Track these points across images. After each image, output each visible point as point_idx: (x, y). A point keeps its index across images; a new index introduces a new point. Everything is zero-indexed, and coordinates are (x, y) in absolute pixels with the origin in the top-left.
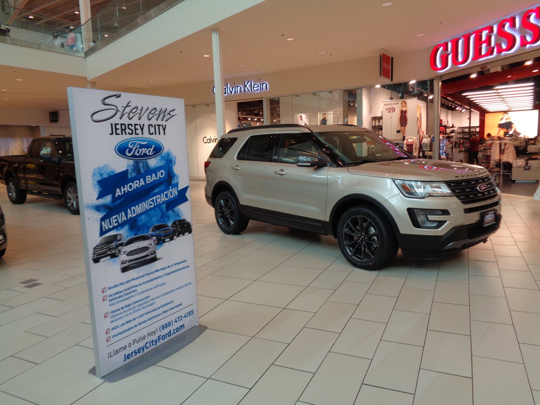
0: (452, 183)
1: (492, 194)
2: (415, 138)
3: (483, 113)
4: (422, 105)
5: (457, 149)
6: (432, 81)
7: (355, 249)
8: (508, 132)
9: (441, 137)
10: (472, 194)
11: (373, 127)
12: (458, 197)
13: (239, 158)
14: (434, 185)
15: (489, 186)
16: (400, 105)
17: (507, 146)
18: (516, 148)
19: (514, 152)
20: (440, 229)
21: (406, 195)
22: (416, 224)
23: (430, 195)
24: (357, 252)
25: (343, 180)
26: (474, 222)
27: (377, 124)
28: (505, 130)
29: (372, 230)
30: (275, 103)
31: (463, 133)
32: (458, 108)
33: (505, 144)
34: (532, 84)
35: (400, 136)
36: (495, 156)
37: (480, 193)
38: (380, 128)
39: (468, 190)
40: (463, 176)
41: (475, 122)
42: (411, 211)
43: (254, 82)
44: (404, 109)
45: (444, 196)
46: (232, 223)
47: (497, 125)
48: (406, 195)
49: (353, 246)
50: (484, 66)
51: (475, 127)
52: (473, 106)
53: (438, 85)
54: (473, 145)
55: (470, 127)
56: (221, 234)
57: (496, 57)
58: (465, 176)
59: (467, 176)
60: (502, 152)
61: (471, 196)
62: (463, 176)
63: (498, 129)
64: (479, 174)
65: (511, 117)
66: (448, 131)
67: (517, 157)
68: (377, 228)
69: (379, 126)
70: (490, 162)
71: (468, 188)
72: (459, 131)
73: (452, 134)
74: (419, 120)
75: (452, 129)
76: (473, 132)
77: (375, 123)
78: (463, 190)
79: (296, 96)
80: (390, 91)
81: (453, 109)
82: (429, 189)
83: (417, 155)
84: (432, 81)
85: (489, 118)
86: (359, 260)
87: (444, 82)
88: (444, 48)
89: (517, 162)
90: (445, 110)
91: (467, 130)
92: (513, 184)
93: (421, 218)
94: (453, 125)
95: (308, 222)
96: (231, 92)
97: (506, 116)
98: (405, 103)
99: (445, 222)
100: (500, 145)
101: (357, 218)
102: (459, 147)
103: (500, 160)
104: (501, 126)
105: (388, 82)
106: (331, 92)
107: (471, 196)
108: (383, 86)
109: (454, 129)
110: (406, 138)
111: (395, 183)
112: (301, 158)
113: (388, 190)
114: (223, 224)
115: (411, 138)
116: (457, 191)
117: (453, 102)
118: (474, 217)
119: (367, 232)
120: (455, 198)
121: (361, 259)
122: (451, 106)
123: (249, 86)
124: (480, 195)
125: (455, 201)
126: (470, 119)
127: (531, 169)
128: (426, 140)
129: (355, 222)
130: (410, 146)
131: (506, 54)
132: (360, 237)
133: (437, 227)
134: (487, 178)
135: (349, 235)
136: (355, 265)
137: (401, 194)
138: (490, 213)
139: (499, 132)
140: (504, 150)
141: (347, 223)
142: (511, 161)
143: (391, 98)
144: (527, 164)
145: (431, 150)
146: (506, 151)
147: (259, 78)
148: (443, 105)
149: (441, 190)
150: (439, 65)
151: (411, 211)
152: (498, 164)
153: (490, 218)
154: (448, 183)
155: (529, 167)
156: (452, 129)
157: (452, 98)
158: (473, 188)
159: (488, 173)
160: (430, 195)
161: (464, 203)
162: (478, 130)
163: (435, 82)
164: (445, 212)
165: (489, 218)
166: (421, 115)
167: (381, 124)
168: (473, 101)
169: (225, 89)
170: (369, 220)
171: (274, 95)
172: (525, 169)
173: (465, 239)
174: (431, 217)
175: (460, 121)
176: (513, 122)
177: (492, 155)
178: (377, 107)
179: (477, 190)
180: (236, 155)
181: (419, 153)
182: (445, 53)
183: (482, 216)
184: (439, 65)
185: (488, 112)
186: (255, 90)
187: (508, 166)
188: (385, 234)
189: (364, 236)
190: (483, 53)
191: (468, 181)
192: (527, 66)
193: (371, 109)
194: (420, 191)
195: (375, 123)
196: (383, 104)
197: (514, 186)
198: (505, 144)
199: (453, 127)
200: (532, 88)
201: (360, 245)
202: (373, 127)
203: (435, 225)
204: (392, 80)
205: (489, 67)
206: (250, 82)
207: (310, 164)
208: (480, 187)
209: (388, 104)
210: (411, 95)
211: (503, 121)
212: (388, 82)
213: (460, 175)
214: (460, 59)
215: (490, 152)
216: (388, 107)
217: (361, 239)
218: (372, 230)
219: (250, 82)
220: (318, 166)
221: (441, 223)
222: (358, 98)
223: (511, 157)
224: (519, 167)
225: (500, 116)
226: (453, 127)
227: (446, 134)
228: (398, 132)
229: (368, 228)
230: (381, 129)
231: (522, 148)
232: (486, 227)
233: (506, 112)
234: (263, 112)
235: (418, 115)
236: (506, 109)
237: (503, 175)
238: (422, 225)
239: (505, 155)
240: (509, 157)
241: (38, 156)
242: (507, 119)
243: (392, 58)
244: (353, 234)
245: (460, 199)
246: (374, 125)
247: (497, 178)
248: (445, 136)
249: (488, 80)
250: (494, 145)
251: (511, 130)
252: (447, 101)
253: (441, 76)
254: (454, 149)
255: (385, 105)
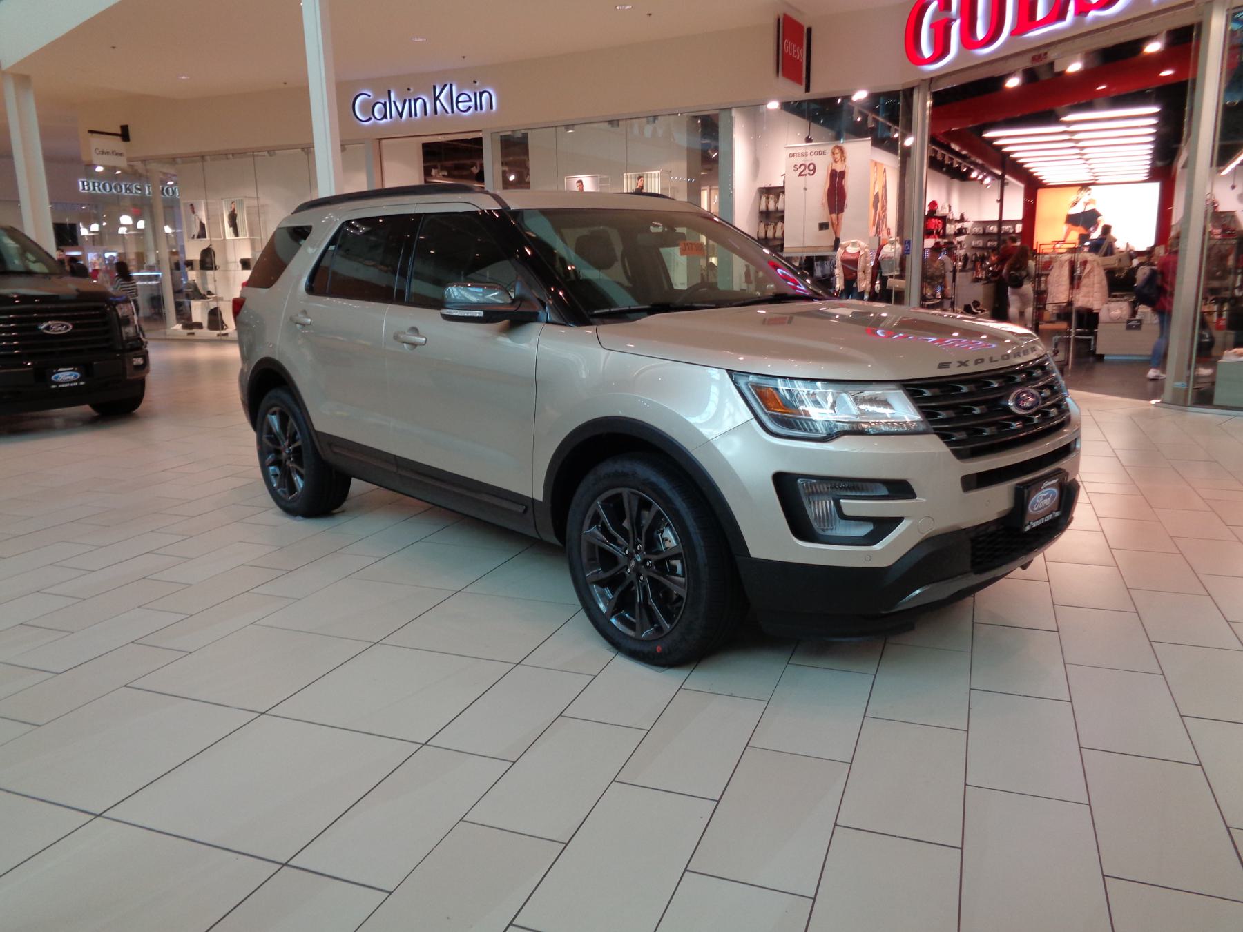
0: (928, 386)
1: (1053, 419)
2: (862, 244)
3: (1033, 186)
4: (889, 162)
5: (970, 274)
6: (908, 93)
7: (617, 594)
8: (1088, 235)
9: (929, 243)
10: (989, 425)
11: (761, 213)
12: (944, 436)
13: (311, 289)
14: (868, 393)
15: (1046, 393)
16: (828, 156)
17: (1088, 267)
18: (1110, 273)
19: (1105, 282)
20: (877, 547)
21: (771, 426)
22: (801, 527)
23: (856, 431)
24: (623, 604)
25: (595, 370)
26: (995, 517)
27: (772, 207)
28: (1082, 230)
29: (669, 539)
30: (515, 149)
31: (985, 235)
32: (974, 175)
33: (1085, 263)
34: (1155, 109)
35: (827, 238)
36: (1059, 292)
37: (1017, 418)
38: (779, 216)
39: (977, 410)
40: (963, 364)
41: (1014, 209)
42: (783, 482)
43: (458, 89)
44: (839, 168)
45: (900, 432)
46: (300, 483)
47: (1064, 218)
48: (771, 426)
49: (612, 583)
50: (1042, 52)
51: (1014, 222)
52: (1009, 167)
53: (923, 106)
54: (1007, 263)
55: (1000, 223)
56: (274, 515)
57: (1074, 25)
58: (971, 363)
59: (977, 362)
60: (1075, 281)
61: (987, 432)
62: (963, 364)
63: (1065, 227)
64: (1017, 355)
65: (1098, 199)
66: (951, 229)
67: (1110, 296)
68: (683, 534)
69: (777, 211)
70: (1044, 308)
71: (977, 404)
72: (976, 230)
73: (960, 238)
74: (879, 201)
75: (959, 226)
76: (1007, 233)
77: (767, 203)
78: (963, 412)
79: (568, 127)
80: (803, 122)
81: (964, 177)
82: (847, 410)
83: (868, 288)
84: (908, 93)
85: (1045, 201)
86: (631, 633)
87: (941, 99)
88: (939, 4)
89: (1109, 310)
90: (944, 178)
91: (994, 229)
92: (1098, 366)
93: (818, 508)
94: (962, 216)
95: (496, 501)
96: (401, 114)
97: (1085, 196)
98: (842, 151)
99: (896, 521)
100: (1072, 265)
101: (620, 495)
102: (974, 269)
103: (1070, 303)
104: (1072, 220)
105: (797, 93)
106: (655, 117)
107: (987, 432)
108: (792, 108)
109: (966, 225)
110: (843, 243)
111: (735, 383)
112: (455, 292)
113: (711, 412)
114: (279, 486)
115: (854, 244)
116: (943, 415)
117: (964, 157)
118: (994, 503)
119: (652, 544)
120: (935, 438)
121: (631, 626)
122: (959, 168)
123: (446, 98)
124: (1016, 425)
125: (934, 446)
126: (1001, 201)
127: (1144, 327)
128: (892, 250)
129: (616, 508)
130: (851, 264)
131: (1097, 19)
132: (631, 556)
133: (872, 539)
134: (1041, 366)
135: (603, 552)
136: (617, 643)
137: (755, 423)
138: (1046, 484)
139: (1067, 234)
140: (1080, 278)
141: (591, 513)
142: (1096, 305)
143: (808, 140)
144: (1134, 313)
145: (901, 276)
146: (1084, 282)
147: (473, 78)
148: (935, 164)
149: (887, 411)
150: (927, 52)
151: (783, 482)
152: (1065, 313)
153: (1046, 502)
154: (913, 389)
155: (1139, 321)
156: (959, 226)
157: (963, 147)
158: (995, 405)
159: (1041, 349)
160: (856, 431)
161: (960, 455)
162: (1019, 228)
163: (915, 96)
164: (900, 489)
165: (1043, 500)
166: (885, 187)
167: (780, 207)
168: (1009, 153)
169: (385, 105)
170: (656, 507)
171: (511, 124)
172: (1129, 328)
173: (964, 573)
174: (851, 506)
175: (979, 206)
176: (1099, 210)
177: (1051, 289)
178: (772, 161)
179: (1007, 410)
180: (304, 281)
181: (873, 283)
182: (943, 16)
183: (1021, 499)
184: (927, 52)
185: (1045, 186)
186: (464, 109)
187: (1089, 319)
188: (701, 553)
189: (650, 557)
190: (1041, 14)
191: (979, 381)
192: (1150, 56)
193: (756, 165)
194: (820, 414)
195: (767, 203)
196: (787, 153)
197: (1100, 371)
198: (1085, 263)
199: (962, 219)
200: (1154, 121)
201: (632, 584)
202: (761, 213)
203: (863, 530)
204: (808, 89)
205: (1052, 55)
206: (448, 88)
207: (479, 314)
208: (1018, 400)
209: (798, 155)
210: (858, 131)
211: (1078, 209)
212: (797, 93)
213: (953, 358)
214: (981, 34)
215: (1046, 282)
216: (799, 161)
217: (633, 563)
218: (669, 539)
219: (448, 88)
220: (514, 319)
221: (883, 526)
222: (721, 130)
223: (1098, 295)
224: (1115, 321)
225: (1072, 195)
226: (962, 219)
227: (944, 236)
228: (823, 226)
229: (656, 525)
230: (782, 219)
231: (1123, 275)
232: (1032, 529)
233: (1085, 186)
234: (482, 166)
235: (878, 189)
236: (1085, 178)
237: (1076, 340)
238: (820, 532)
239: (1083, 290)
240: (1092, 295)
241: (940, 284)
242: (1087, 204)
243: (809, 30)
244: (611, 547)
245: (949, 444)
246: (763, 207)
247: (1061, 348)
248: (942, 241)
249: (1046, 98)
250: (1056, 265)
251: (1095, 229)
252: (948, 155)
253: (932, 80)
254: (958, 275)
255: (792, 155)
